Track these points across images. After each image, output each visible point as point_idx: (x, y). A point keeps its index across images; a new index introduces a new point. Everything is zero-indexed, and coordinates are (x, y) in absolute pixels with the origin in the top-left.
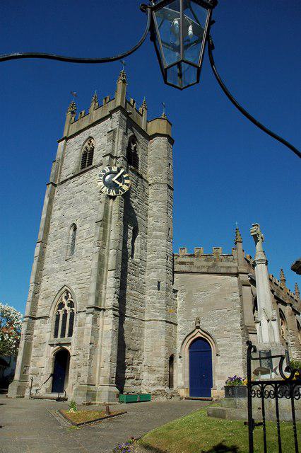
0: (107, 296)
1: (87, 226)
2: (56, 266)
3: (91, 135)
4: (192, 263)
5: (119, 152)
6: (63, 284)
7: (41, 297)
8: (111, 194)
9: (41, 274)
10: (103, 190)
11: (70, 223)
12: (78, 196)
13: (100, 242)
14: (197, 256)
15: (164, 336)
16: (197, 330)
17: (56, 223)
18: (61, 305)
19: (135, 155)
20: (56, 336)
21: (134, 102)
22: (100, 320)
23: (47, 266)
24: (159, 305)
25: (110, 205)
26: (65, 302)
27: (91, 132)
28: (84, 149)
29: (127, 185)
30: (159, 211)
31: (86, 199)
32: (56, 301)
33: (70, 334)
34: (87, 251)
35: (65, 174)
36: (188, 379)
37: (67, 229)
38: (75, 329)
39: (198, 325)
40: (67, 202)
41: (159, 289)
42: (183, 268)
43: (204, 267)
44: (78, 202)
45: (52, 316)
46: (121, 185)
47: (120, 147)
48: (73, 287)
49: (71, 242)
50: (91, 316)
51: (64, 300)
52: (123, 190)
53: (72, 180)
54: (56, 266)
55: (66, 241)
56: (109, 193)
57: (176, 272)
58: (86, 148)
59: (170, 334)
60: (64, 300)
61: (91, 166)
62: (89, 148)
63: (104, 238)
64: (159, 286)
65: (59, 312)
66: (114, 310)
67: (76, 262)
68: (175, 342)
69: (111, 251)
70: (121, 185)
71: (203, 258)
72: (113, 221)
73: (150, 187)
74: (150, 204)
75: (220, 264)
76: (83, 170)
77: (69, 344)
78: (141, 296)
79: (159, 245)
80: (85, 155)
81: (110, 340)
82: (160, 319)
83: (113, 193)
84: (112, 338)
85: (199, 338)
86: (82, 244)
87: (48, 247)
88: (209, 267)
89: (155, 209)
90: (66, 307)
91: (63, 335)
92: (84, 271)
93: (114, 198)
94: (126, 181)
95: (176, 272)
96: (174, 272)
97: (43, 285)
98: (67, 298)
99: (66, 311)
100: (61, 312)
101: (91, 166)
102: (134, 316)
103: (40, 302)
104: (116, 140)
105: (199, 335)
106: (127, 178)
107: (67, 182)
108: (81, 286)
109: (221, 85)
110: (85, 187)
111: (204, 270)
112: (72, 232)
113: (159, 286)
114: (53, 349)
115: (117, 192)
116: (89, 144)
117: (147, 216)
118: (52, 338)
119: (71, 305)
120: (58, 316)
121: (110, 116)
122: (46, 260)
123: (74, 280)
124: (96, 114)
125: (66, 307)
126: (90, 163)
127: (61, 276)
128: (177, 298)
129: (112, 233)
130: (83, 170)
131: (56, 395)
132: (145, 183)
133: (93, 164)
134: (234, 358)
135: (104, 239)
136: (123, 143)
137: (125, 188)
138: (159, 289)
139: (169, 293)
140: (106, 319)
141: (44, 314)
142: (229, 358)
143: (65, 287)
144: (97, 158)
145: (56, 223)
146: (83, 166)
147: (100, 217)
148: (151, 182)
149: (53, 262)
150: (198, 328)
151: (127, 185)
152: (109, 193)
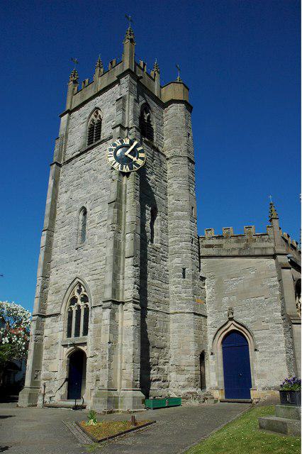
2: (65, 256)
3: (97, 106)
4: (220, 246)
6: (74, 276)
7: (50, 292)
8: (125, 170)
9: (49, 266)
10: (115, 166)
11: (79, 206)
13: (114, 225)
14: (226, 238)
16: (231, 322)
17: (63, 207)
18: (74, 300)
20: (69, 335)
21: (144, 65)
22: (119, 315)
23: (56, 257)
25: (124, 183)
27: (98, 102)
29: (142, 159)
31: (95, 178)
32: (67, 295)
33: (86, 333)
34: (100, 237)
35: (70, 152)
36: (222, 379)
37: (75, 214)
38: (91, 326)
39: (231, 316)
40: (75, 183)
41: (184, 277)
43: (234, 249)
44: (86, 182)
45: (64, 312)
46: (135, 159)
47: (132, 117)
48: (86, 279)
49: (81, 228)
50: (108, 311)
51: (76, 294)
52: (138, 166)
54: (65, 256)
55: (75, 227)
56: (122, 169)
57: (203, 257)
58: (93, 120)
59: (200, 328)
60: (76, 294)
61: (99, 141)
62: (96, 120)
63: (119, 220)
64: (184, 274)
65: (71, 308)
67: (88, 250)
70: (135, 159)
71: (233, 240)
72: (128, 201)
73: (168, 162)
74: (169, 181)
75: (253, 245)
76: (91, 146)
77: (85, 344)
81: (132, 338)
82: (187, 310)
84: (134, 334)
85: (233, 331)
87: (55, 235)
89: (175, 186)
91: (77, 334)
93: (127, 174)
94: (141, 155)
95: (203, 257)
97: (53, 278)
98: (79, 291)
99: (79, 306)
100: (74, 308)
101: (99, 141)
102: (158, 309)
103: (49, 298)
104: (127, 109)
105: (232, 328)
108: (95, 277)
110: (93, 165)
111: (236, 253)
112: (81, 216)
113: (184, 274)
114: (66, 350)
116: (96, 116)
117: (166, 194)
118: (65, 338)
119: (85, 299)
120: (70, 313)
121: (118, 82)
122: (54, 249)
124: (101, 82)
126: (98, 137)
127: (72, 266)
128: (206, 287)
129: (128, 215)
130: (91, 146)
131: (72, 403)
133: (102, 138)
135: (119, 222)
137: (140, 162)
138: (184, 277)
140: (126, 313)
141: (55, 311)
142: (270, 353)
143: (77, 280)
144: (106, 131)
145: (63, 207)
146: (90, 141)
147: (113, 197)
149: (62, 252)
150: (231, 319)
151: (142, 159)
152: (122, 169)
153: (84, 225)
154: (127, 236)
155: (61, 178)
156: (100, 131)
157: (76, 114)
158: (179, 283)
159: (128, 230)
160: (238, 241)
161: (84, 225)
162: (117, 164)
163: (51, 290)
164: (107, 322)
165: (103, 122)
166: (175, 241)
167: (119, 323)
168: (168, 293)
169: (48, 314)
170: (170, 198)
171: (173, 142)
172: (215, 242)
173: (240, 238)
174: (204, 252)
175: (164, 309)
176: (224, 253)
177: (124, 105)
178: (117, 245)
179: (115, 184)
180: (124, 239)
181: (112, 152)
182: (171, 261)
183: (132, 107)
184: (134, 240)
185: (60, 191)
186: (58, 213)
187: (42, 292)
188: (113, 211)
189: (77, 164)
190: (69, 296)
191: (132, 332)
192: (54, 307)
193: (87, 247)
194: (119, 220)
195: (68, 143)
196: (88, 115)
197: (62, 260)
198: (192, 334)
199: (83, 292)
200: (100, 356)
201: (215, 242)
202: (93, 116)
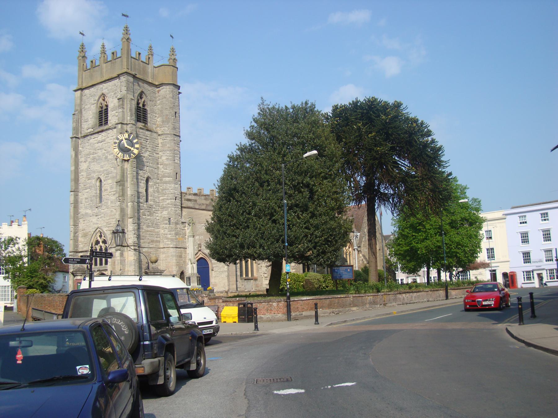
0: (129, 236)
1: (110, 181)
2: (89, 211)
3: (105, 91)
4: (196, 201)
5: (129, 118)
6: (96, 226)
7: (80, 235)
8: (125, 158)
9: (77, 217)
10: (119, 156)
11: (95, 175)
12: (100, 153)
13: (120, 198)
14: (199, 196)
15: (174, 258)
16: (200, 252)
17: (84, 174)
18: (97, 242)
19: (145, 111)
22: (125, 254)
23: (82, 211)
24: (170, 236)
25: (126, 167)
26: (100, 240)
27: (105, 88)
28: (99, 105)
29: (137, 149)
30: (167, 159)
31: (106, 158)
32: (93, 239)
34: (112, 202)
37: (93, 181)
39: (200, 249)
41: (170, 224)
42: (190, 204)
43: (203, 204)
46: (132, 149)
47: (129, 114)
48: (105, 229)
49: (98, 192)
50: (119, 252)
51: (99, 239)
52: (134, 154)
53: (93, 137)
54: (89, 211)
55: (94, 192)
56: (123, 157)
57: (185, 207)
59: (180, 257)
60: (99, 239)
63: (123, 194)
64: (169, 221)
66: (134, 246)
67: (104, 210)
68: (185, 262)
69: (129, 204)
70: (132, 149)
71: (203, 198)
72: (129, 179)
73: (159, 137)
74: (160, 153)
77: (106, 270)
78: (157, 230)
79: (168, 189)
80: (101, 112)
81: (133, 267)
82: (172, 246)
83: (127, 157)
84: (134, 265)
85: (201, 258)
86: (108, 196)
87: (80, 194)
88: (207, 205)
89: (164, 158)
90: (101, 243)
92: (111, 217)
93: (128, 160)
94: (137, 146)
95: (185, 207)
96: (182, 207)
97: (81, 226)
98: (101, 236)
99: (101, 247)
102: (152, 246)
103: (80, 239)
104: (125, 107)
105: (201, 256)
106: (137, 143)
107: (89, 137)
109: (58, 379)
111: (204, 207)
112: (98, 184)
113: (169, 221)
115: (130, 156)
117: (158, 164)
122: (80, 205)
123: (105, 224)
125: (101, 243)
126: (106, 123)
127: (94, 219)
128: (186, 228)
129: (129, 189)
132: (155, 135)
134: (222, 272)
135: (123, 195)
136: (131, 110)
137: (136, 151)
138: (170, 224)
139: (178, 226)
140: (130, 252)
142: (219, 272)
143: (99, 229)
144: (113, 119)
145: (84, 174)
146: (101, 125)
147: (119, 178)
148: (160, 133)
149: (86, 208)
150: (200, 250)
151: (137, 149)
152: (123, 157)
153: (101, 190)
154: (129, 204)
155: (80, 149)
156: (108, 113)
157: (86, 91)
158: (166, 228)
159: (129, 200)
160: (206, 199)
161: (101, 190)
162: (120, 153)
163: (80, 234)
164: (119, 258)
165: (109, 109)
166: (164, 199)
167: (126, 258)
168: (159, 235)
169: (80, 250)
170: (161, 167)
171: (163, 122)
172: (193, 197)
173: (207, 197)
174: (186, 203)
175: (156, 245)
176: (197, 207)
177: (123, 105)
178: (122, 211)
179: (119, 168)
180: (127, 206)
181: (116, 145)
182: (161, 213)
183: (129, 106)
184: (133, 207)
185: (81, 160)
186: (80, 177)
187: (74, 236)
188: (119, 188)
189: (92, 141)
190: (93, 241)
191: (133, 263)
192: (84, 246)
193: (104, 207)
194: (123, 194)
195: (83, 118)
196: (97, 98)
197: (86, 214)
198: (175, 261)
199: (103, 238)
200: (254, 198)
201: (193, 197)
202: (101, 100)
